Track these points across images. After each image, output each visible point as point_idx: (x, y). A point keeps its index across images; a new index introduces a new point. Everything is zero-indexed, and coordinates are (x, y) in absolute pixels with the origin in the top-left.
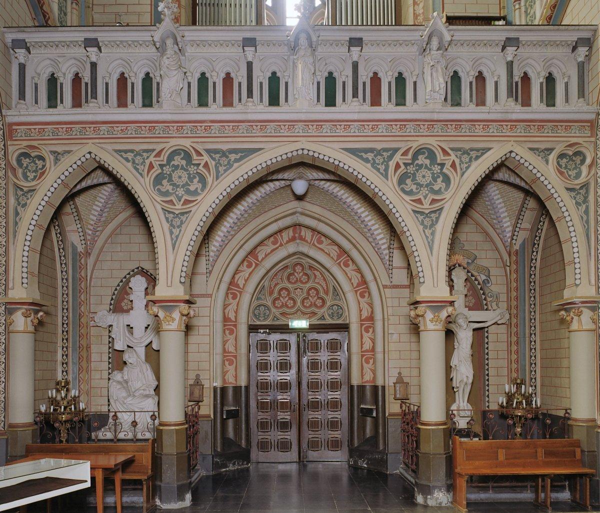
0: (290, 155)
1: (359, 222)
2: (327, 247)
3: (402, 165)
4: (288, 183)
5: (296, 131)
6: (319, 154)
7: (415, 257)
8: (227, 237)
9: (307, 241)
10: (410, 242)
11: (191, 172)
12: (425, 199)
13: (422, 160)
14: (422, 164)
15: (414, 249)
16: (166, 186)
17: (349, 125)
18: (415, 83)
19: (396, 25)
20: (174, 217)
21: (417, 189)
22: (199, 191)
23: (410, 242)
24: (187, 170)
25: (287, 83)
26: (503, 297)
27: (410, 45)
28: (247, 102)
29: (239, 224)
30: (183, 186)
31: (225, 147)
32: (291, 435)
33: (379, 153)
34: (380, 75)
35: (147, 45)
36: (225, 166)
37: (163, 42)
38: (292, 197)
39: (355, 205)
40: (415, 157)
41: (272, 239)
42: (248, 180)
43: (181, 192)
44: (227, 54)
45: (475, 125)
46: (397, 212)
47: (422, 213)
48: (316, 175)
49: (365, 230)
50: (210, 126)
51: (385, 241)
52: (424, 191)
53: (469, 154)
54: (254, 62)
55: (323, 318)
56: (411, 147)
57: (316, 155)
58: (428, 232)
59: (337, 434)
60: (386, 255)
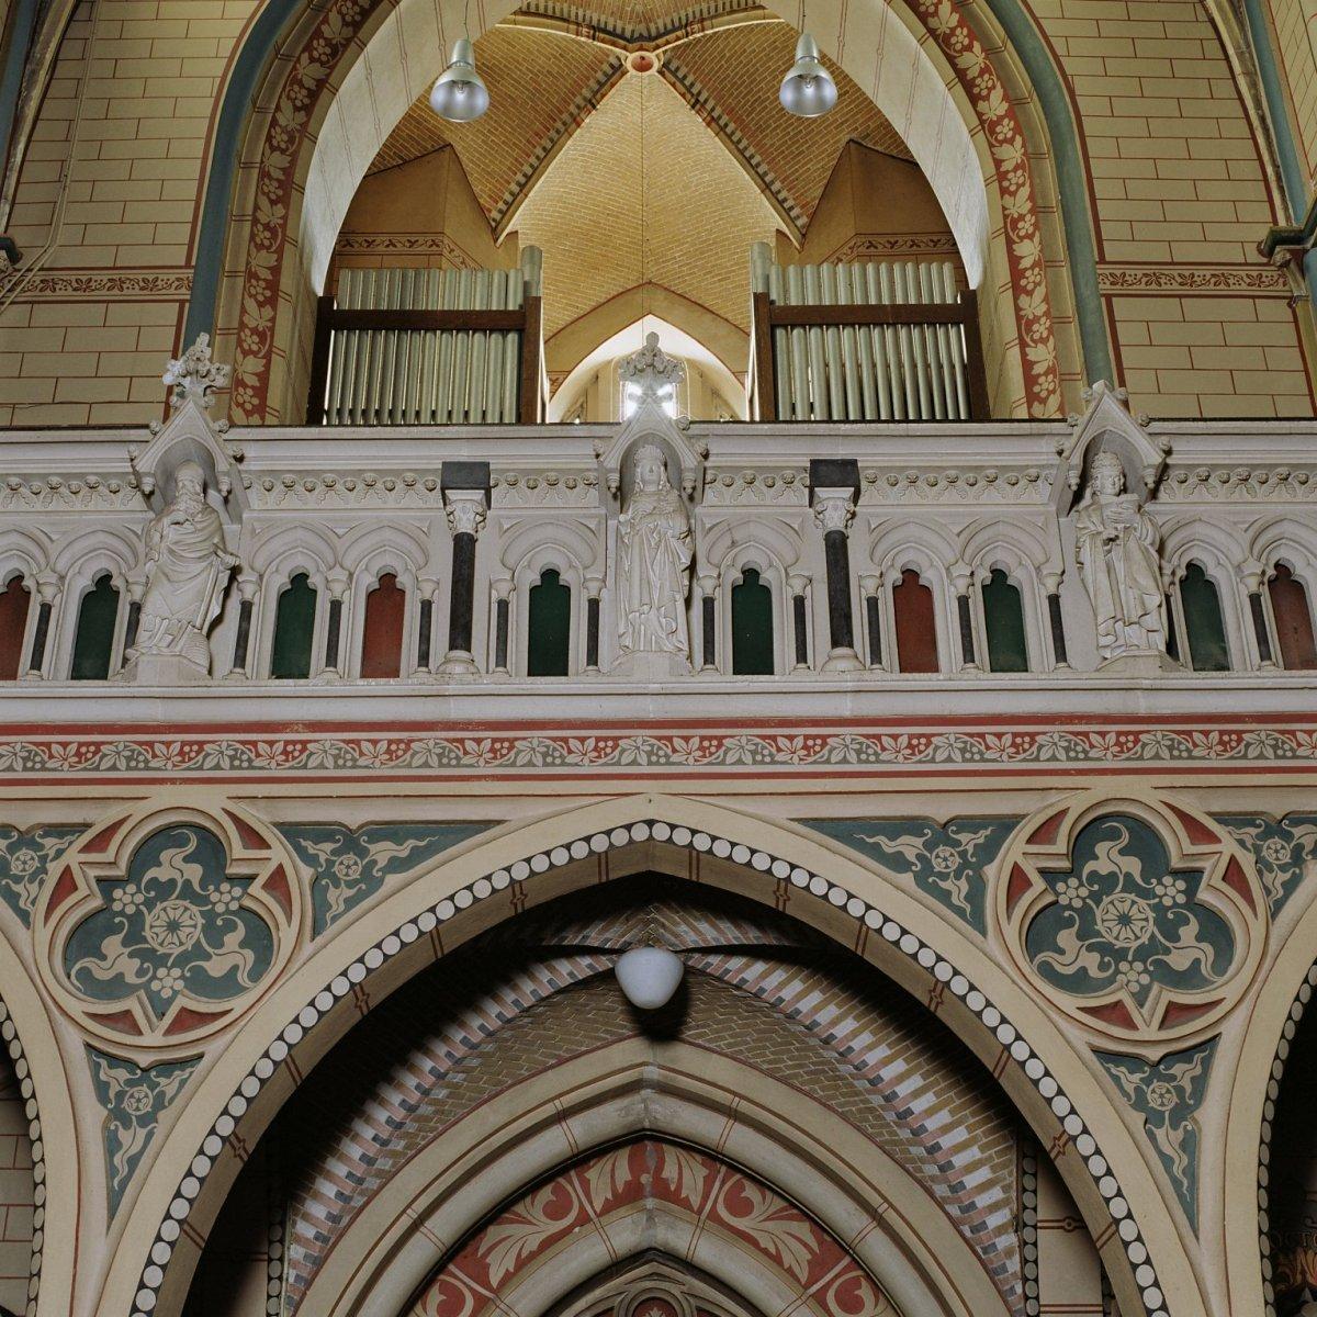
0: (600, 844)
1: (890, 1117)
2: (770, 1225)
3: (1035, 878)
4: (603, 963)
5: (626, 758)
6: (714, 839)
7: (1126, 1244)
8: (360, 1181)
9: (685, 1204)
10: (1097, 1180)
11: (220, 908)
12: (1141, 1005)
13: (1108, 858)
14: (1113, 875)
15: (1118, 1208)
16: (116, 957)
17: (824, 738)
18: (1054, 601)
19: (970, 419)
20: (130, 1083)
21: (1102, 967)
22: (242, 978)
23: (1097, 1180)
24: (204, 900)
25: (594, 605)
27: (1023, 482)
28: (447, 661)
29: (411, 1127)
30: (182, 960)
31: (354, 816)
33: (943, 833)
34: (928, 577)
35: (114, 487)
36: (350, 885)
37: (168, 476)
38: (622, 1021)
39: (870, 1048)
40: (1082, 846)
41: (546, 1194)
42: (435, 936)
43: (169, 981)
44: (389, 514)
45: (1293, 733)
46: (1033, 1055)
47: (1134, 1062)
48: (708, 931)
49: (905, 1134)
50: (304, 743)
51: (996, 1194)
52: (1133, 975)
53: (1288, 836)
54: (480, 535)
56: (1063, 813)
57: (702, 843)
58: (1168, 1138)
60: (1009, 1253)
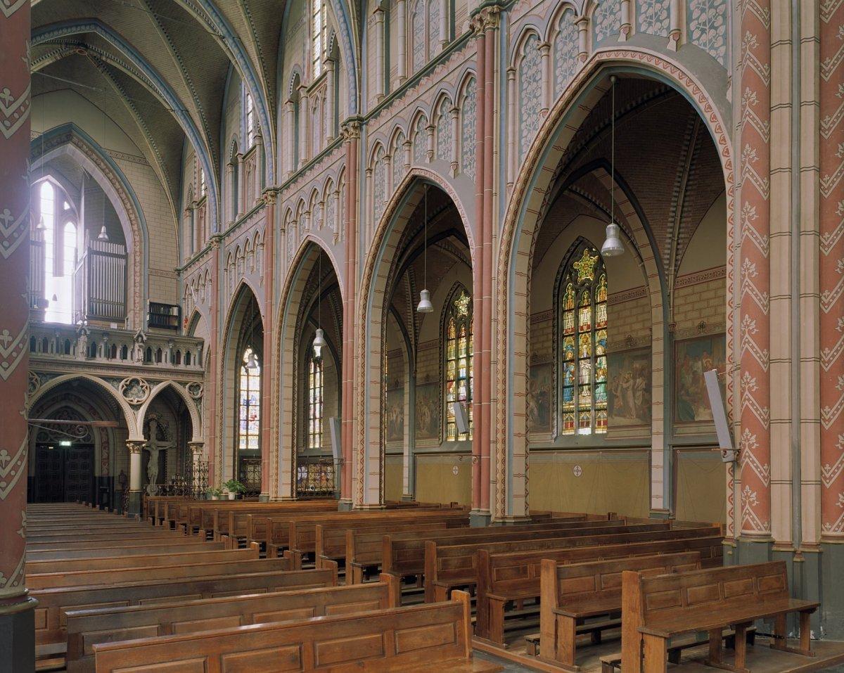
26: (175, 435)
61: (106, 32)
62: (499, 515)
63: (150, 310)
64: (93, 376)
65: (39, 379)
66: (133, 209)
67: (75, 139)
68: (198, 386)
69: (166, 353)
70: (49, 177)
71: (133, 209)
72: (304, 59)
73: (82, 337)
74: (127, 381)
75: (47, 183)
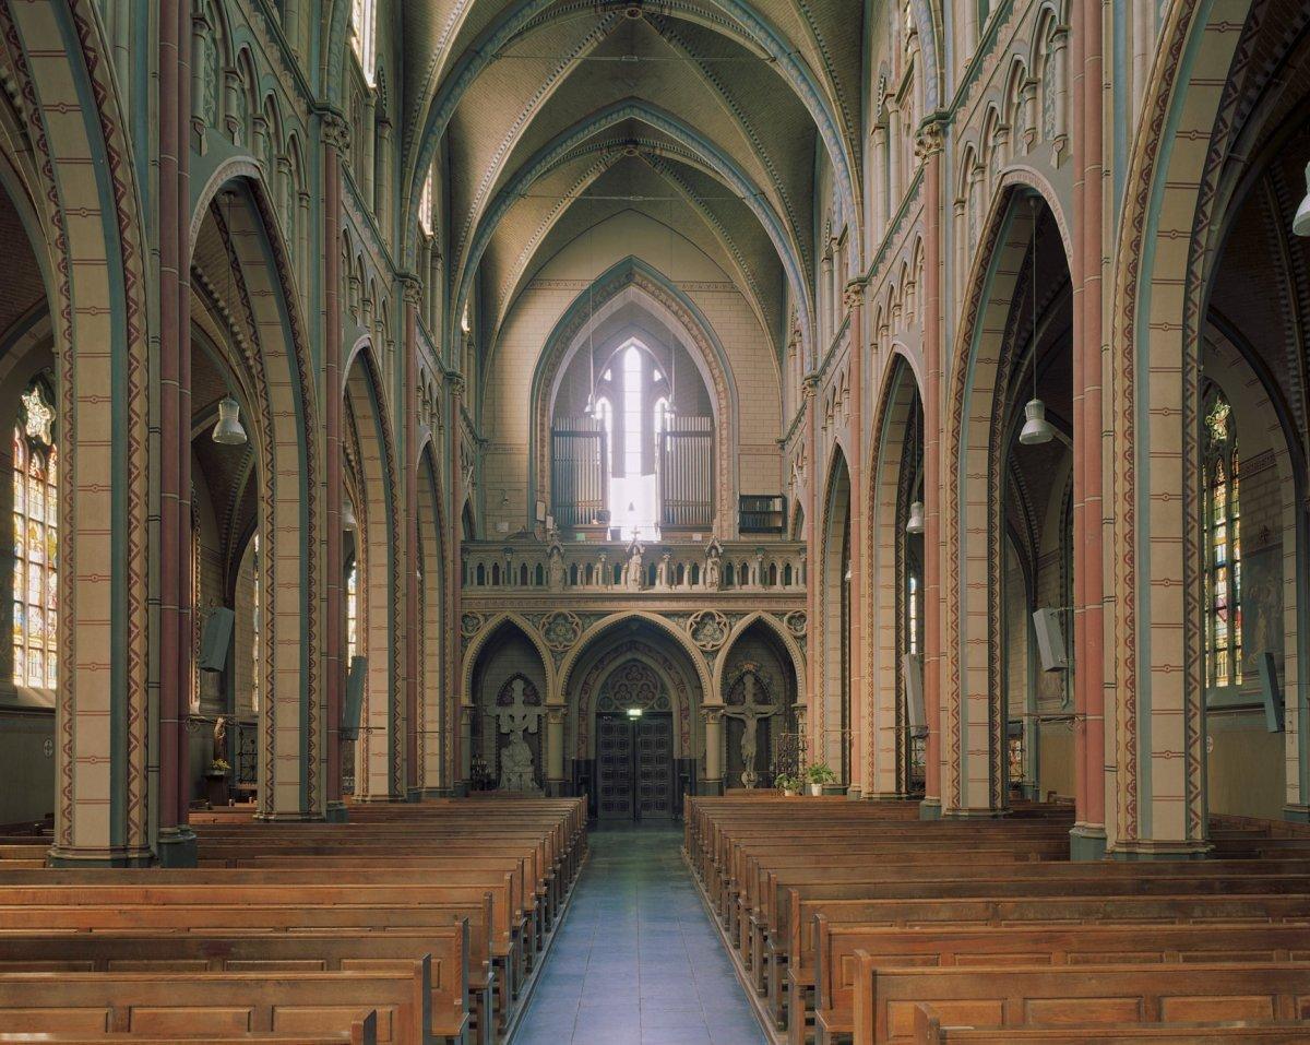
26: (782, 695)
32: (628, 798)
55: (653, 708)
59: (664, 797)
61: (646, 112)
62: (1123, 837)
63: (741, 507)
64: (648, 611)
65: (580, 622)
66: (716, 361)
67: (638, 279)
68: (803, 617)
69: (754, 567)
70: (633, 340)
71: (716, 361)
72: (890, 49)
73: (634, 558)
74: (697, 617)
75: (633, 348)
